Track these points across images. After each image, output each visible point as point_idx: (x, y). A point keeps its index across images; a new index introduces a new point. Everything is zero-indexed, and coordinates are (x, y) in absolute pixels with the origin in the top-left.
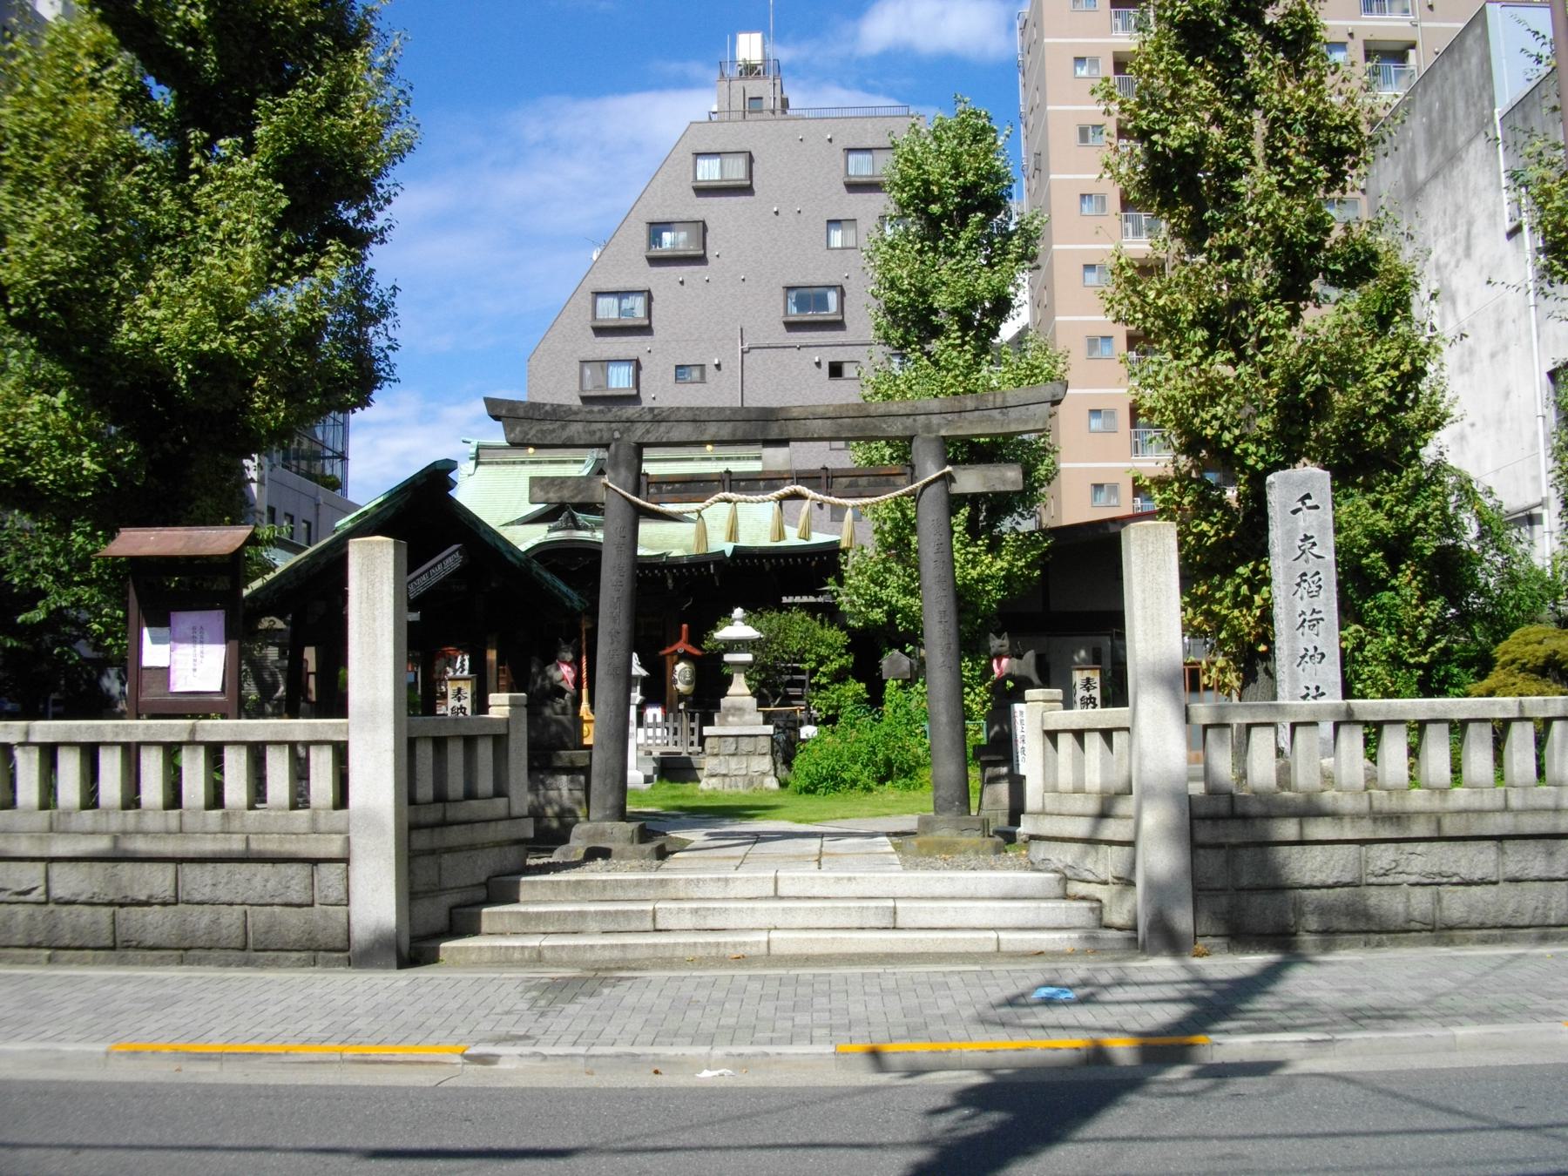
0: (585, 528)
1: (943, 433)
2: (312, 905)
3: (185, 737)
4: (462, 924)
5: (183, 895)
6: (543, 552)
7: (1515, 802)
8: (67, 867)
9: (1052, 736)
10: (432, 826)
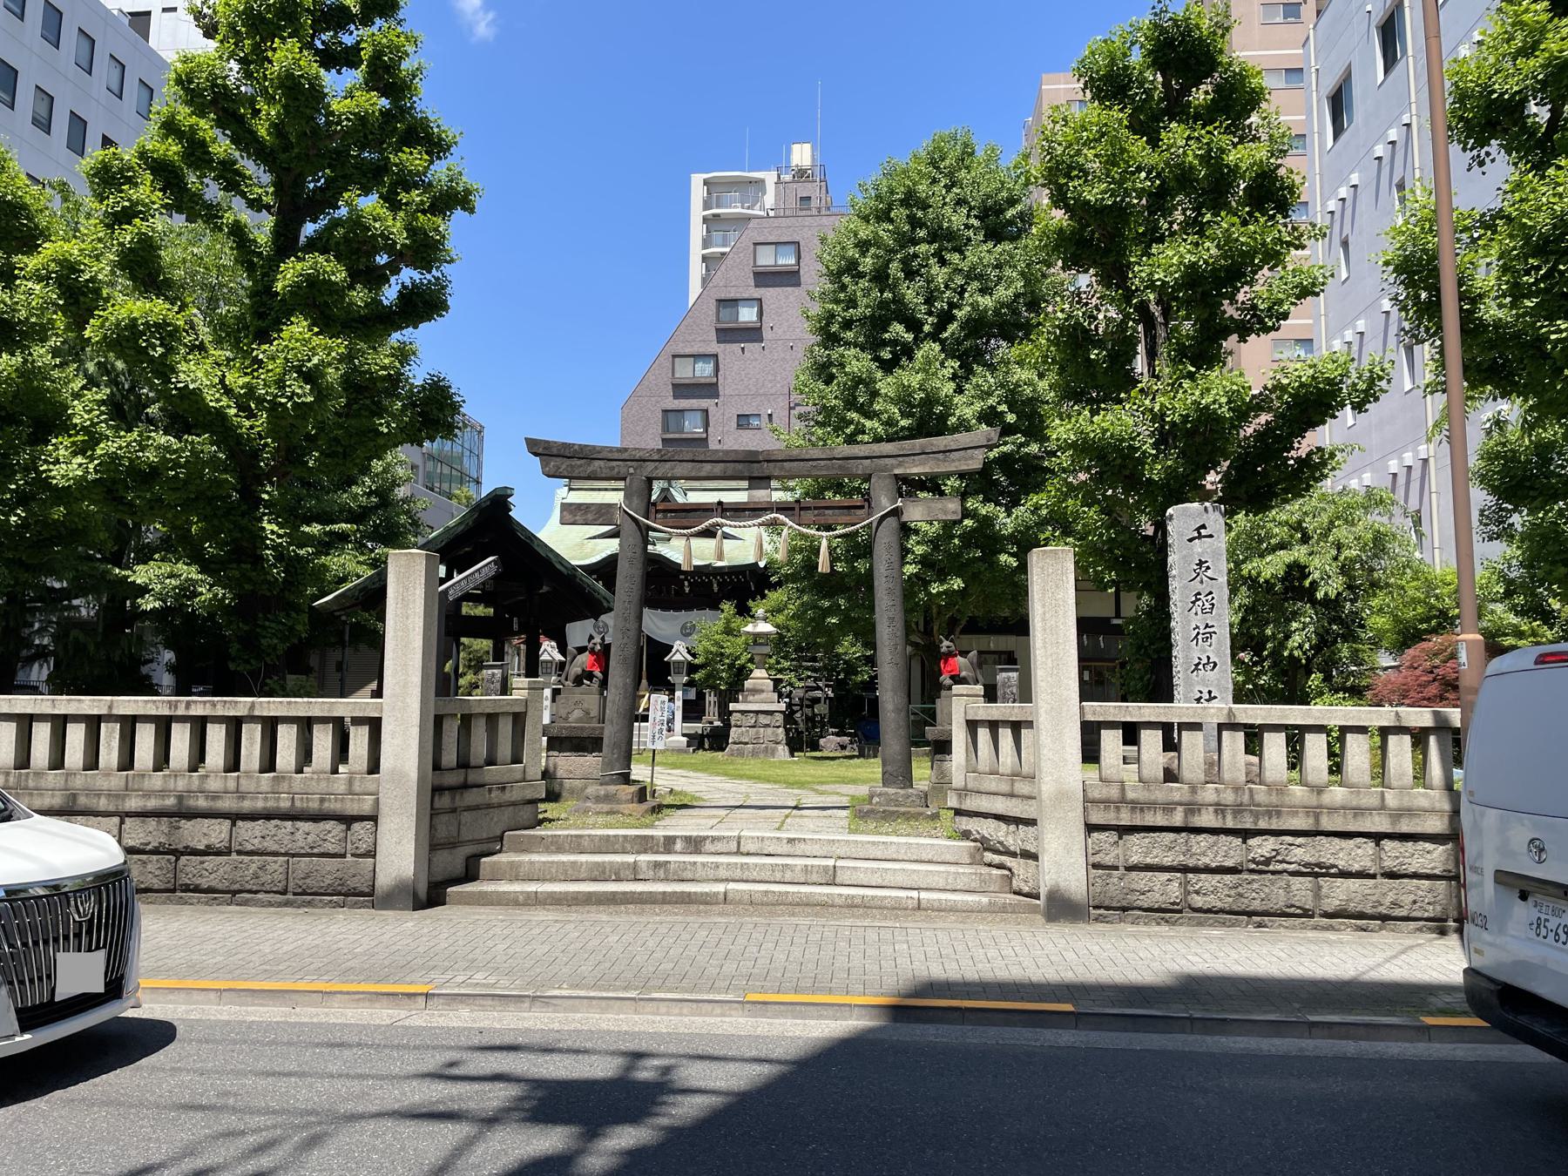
1: (897, 472)
2: (344, 856)
3: (104, 711)
5: (235, 846)
7: (1391, 799)
8: (137, 820)
9: (972, 726)
10: (452, 789)
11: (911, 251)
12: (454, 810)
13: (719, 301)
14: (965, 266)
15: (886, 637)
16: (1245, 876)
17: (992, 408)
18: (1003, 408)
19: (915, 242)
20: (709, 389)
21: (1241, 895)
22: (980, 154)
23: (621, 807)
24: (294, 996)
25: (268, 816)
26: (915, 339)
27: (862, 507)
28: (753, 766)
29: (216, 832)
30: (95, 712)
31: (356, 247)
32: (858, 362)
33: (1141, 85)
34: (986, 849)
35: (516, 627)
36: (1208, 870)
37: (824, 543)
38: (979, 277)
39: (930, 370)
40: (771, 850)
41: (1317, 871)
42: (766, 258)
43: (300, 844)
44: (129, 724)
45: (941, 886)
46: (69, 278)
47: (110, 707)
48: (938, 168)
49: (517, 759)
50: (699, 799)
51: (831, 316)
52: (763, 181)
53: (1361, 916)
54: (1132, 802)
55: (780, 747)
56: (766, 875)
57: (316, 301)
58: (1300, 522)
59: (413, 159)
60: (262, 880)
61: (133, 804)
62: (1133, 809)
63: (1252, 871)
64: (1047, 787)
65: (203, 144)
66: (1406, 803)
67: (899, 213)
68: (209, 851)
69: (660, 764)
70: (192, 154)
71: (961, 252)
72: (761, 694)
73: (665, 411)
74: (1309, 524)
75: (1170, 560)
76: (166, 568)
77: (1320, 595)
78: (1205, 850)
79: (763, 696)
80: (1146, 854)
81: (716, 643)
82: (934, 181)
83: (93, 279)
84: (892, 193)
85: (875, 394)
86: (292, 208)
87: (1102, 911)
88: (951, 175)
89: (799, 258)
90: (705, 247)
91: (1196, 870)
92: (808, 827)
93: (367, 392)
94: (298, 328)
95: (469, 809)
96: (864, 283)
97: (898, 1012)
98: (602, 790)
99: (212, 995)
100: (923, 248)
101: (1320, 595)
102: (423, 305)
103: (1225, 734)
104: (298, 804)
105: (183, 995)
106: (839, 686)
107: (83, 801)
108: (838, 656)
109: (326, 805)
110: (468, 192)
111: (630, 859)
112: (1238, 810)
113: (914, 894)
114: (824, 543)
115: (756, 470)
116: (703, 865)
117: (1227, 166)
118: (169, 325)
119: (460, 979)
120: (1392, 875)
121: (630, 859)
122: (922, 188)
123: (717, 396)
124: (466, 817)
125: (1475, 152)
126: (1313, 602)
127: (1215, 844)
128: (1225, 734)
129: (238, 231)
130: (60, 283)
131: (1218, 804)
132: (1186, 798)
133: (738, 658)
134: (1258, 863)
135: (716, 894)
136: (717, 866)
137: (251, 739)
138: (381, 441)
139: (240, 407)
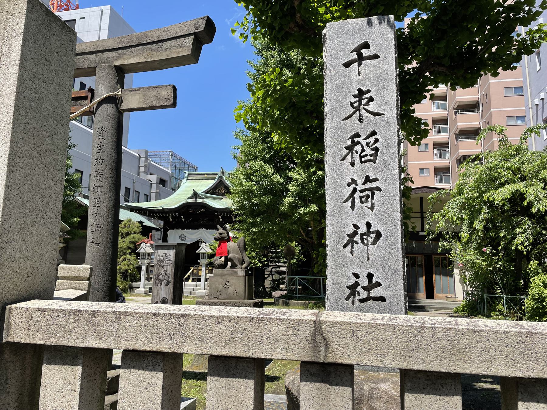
1: (117, 63)
58: (519, 169)
74: (526, 169)
77: (534, 210)
101: (534, 210)
116: (373, 326)
126: (531, 216)
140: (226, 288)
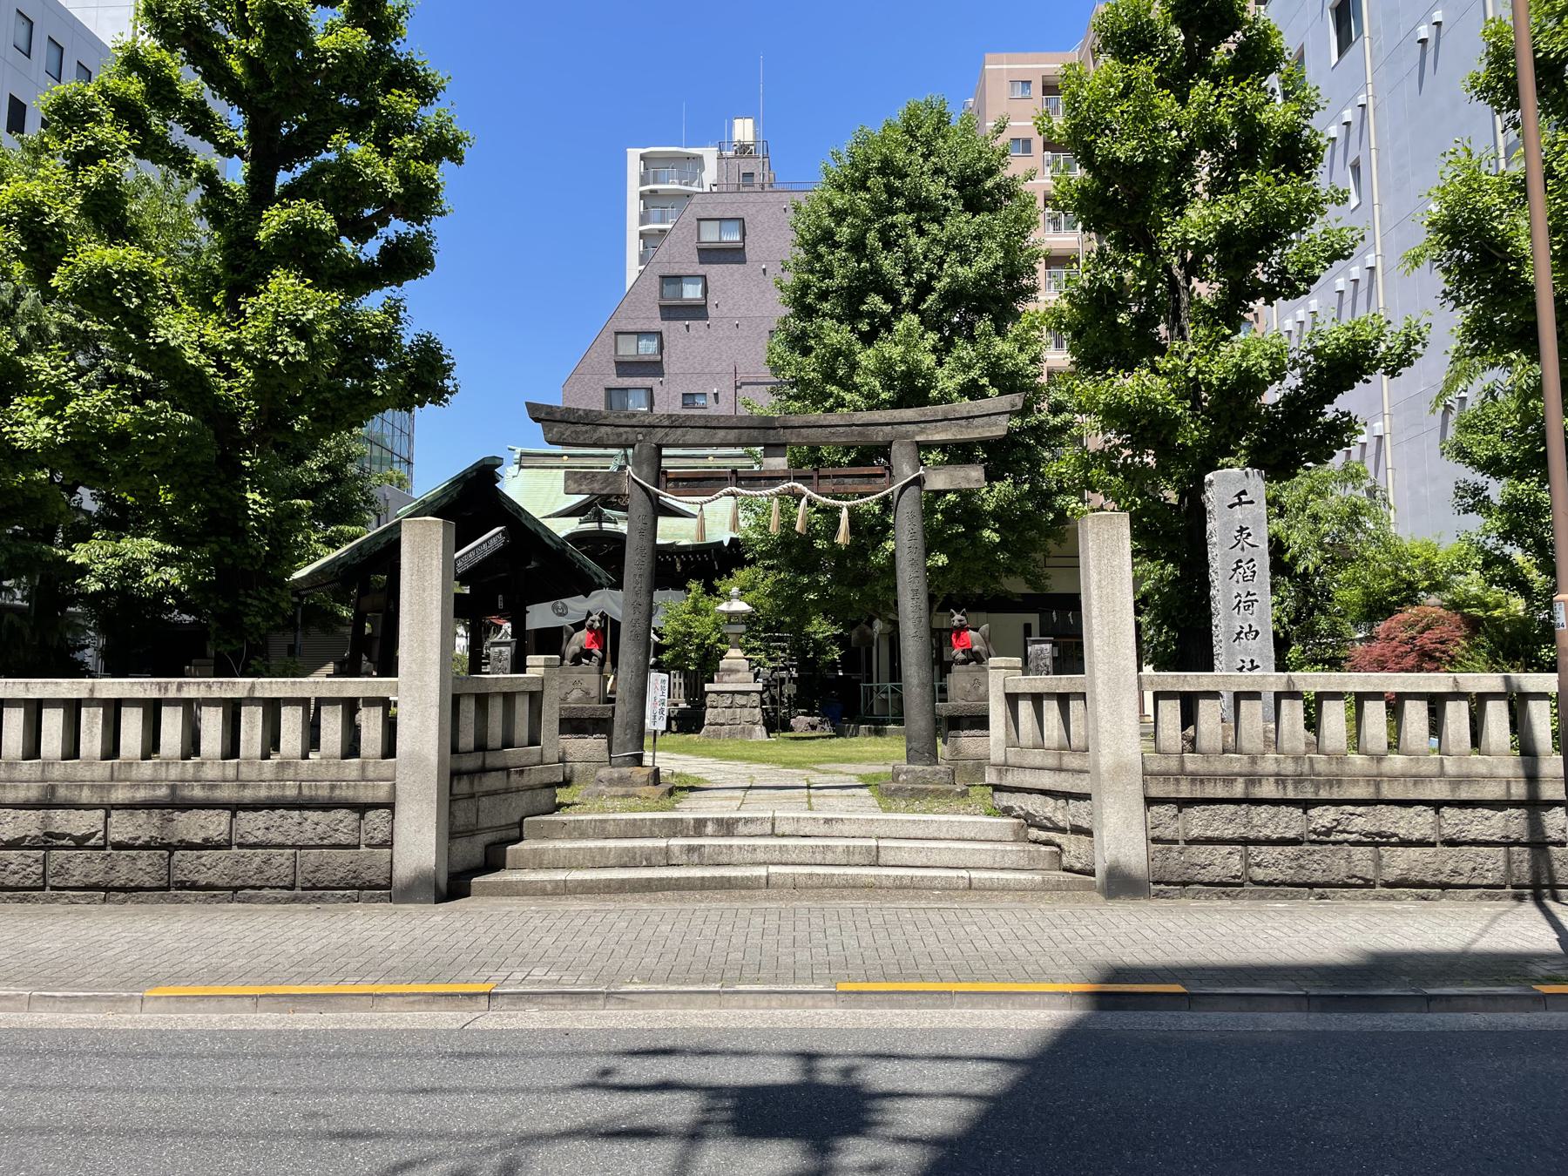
0: (609, 521)
1: (918, 438)
2: (357, 847)
3: (84, 695)
4: (493, 861)
5: (236, 839)
6: (575, 538)
7: (1450, 766)
8: (125, 814)
9: (1012, 699)
10: (471, 773)
11: (889, 220)
12: (472, 796)
13: (663, 277)
14: (943, 236)
15: (910, 609)
16: (1306, 847)
17: (974, 381)
18: (985, 381)
19: (892, 211)
20: (654, 368)
21: (1302, 867)
22: (956, 123)
23: (637, 790)
24: (340, 1000)
25: (272, 805)
26: (893, 311)
27: (883, 476)
28: (732, 746)
29: (215, 824)
30: (75, 696)
31: (347, 195)
32: (837, 334)
33: (1165, 42)
34: (1030, 826)
35: (501, 605)
36: (1269, 842)
37: (844, 514)
38: (958, 248)
39: (908, 342)
40: (807, 831)
41: (1377, 840)
42: (711, 234)
43: (308, 835)
44: (73, 708)
45: (988, 864)
46: (31, 221)
47: (92, 691)
48: (914, 137)
49: (534, 741)
50: (703, 780)
51: (805, 287)
52: (701, 157)
53: (1422, 885)
54: (1192, 774)
55: (757, 728)
56: (806, 857)
57: (302, 250)
59: (401, 101)
60: (267, 874)
61: (120, 795)
62: (1193, 781)
63: (1313, 842)
64: (1106, 760)
65: (169, 83)
66: (1465, 770)
67: (876, 181)
68: (207, 845)
69: (661, 750)
70: (158, 93)
71: (940, 223)
72: (738, 672)
73: (608, 390)
75: (1209, 526)
76: (110, 547)
78: (1266, 822)
79: (740, 675)
80: (1207, 827)
81: (684, 623)
82: (911, 150)
83: (58, 223)
84: (868, 161)
85: (854, 366)
86: (267, 154)
87: (1162, 887)
88: (928, 143)
89: (744, 235)
90: (642, 224)
91: (1257, 842)
92: (835, 805)
93: (359, 347)
94: (284, 285)
95: (488, 794)
96: (841, 253)
97: (1102, 1001)
98: (616, 773)
99: (247, 1002)
100: (900, 218)
101: (1300, 569)
102: (407, 261)
103: (1284, 703)
104: (306, 792)
105: (213, 1003)
106: (804, 665)
107: (62, 793)
108: (808, 635)
109: (337, 792)
110: (457, 140)
111: (662, 843)
112: (1299, 780)
113: (964, 873)
114: (844, 514)
115: (772, 436)
116: (740, 848)
117: (1260, 125)
118: (145, 274)
119: (519, 976)
120: (1451, 843)
121: (662, 843)
122: (900, 155)
123: (662, 375)
124: (485, 802)
125: (1511, 114)
127: (1276, 815)
128: (1284, 703)
129: (209, 178)
130: (21, 227)
131: (1278, 775)
132: (1246, 769)
133: (708, 637)
134: (1319, 834)
135: (758, 878)
136: (754, 849)
137: (251, 722)
138: (374, 404)
139: (221, 366)
140: (976, 689)
